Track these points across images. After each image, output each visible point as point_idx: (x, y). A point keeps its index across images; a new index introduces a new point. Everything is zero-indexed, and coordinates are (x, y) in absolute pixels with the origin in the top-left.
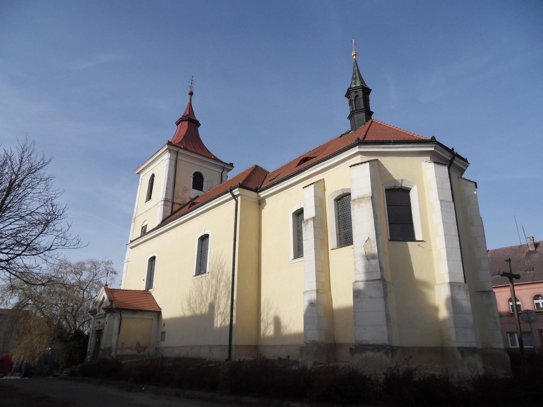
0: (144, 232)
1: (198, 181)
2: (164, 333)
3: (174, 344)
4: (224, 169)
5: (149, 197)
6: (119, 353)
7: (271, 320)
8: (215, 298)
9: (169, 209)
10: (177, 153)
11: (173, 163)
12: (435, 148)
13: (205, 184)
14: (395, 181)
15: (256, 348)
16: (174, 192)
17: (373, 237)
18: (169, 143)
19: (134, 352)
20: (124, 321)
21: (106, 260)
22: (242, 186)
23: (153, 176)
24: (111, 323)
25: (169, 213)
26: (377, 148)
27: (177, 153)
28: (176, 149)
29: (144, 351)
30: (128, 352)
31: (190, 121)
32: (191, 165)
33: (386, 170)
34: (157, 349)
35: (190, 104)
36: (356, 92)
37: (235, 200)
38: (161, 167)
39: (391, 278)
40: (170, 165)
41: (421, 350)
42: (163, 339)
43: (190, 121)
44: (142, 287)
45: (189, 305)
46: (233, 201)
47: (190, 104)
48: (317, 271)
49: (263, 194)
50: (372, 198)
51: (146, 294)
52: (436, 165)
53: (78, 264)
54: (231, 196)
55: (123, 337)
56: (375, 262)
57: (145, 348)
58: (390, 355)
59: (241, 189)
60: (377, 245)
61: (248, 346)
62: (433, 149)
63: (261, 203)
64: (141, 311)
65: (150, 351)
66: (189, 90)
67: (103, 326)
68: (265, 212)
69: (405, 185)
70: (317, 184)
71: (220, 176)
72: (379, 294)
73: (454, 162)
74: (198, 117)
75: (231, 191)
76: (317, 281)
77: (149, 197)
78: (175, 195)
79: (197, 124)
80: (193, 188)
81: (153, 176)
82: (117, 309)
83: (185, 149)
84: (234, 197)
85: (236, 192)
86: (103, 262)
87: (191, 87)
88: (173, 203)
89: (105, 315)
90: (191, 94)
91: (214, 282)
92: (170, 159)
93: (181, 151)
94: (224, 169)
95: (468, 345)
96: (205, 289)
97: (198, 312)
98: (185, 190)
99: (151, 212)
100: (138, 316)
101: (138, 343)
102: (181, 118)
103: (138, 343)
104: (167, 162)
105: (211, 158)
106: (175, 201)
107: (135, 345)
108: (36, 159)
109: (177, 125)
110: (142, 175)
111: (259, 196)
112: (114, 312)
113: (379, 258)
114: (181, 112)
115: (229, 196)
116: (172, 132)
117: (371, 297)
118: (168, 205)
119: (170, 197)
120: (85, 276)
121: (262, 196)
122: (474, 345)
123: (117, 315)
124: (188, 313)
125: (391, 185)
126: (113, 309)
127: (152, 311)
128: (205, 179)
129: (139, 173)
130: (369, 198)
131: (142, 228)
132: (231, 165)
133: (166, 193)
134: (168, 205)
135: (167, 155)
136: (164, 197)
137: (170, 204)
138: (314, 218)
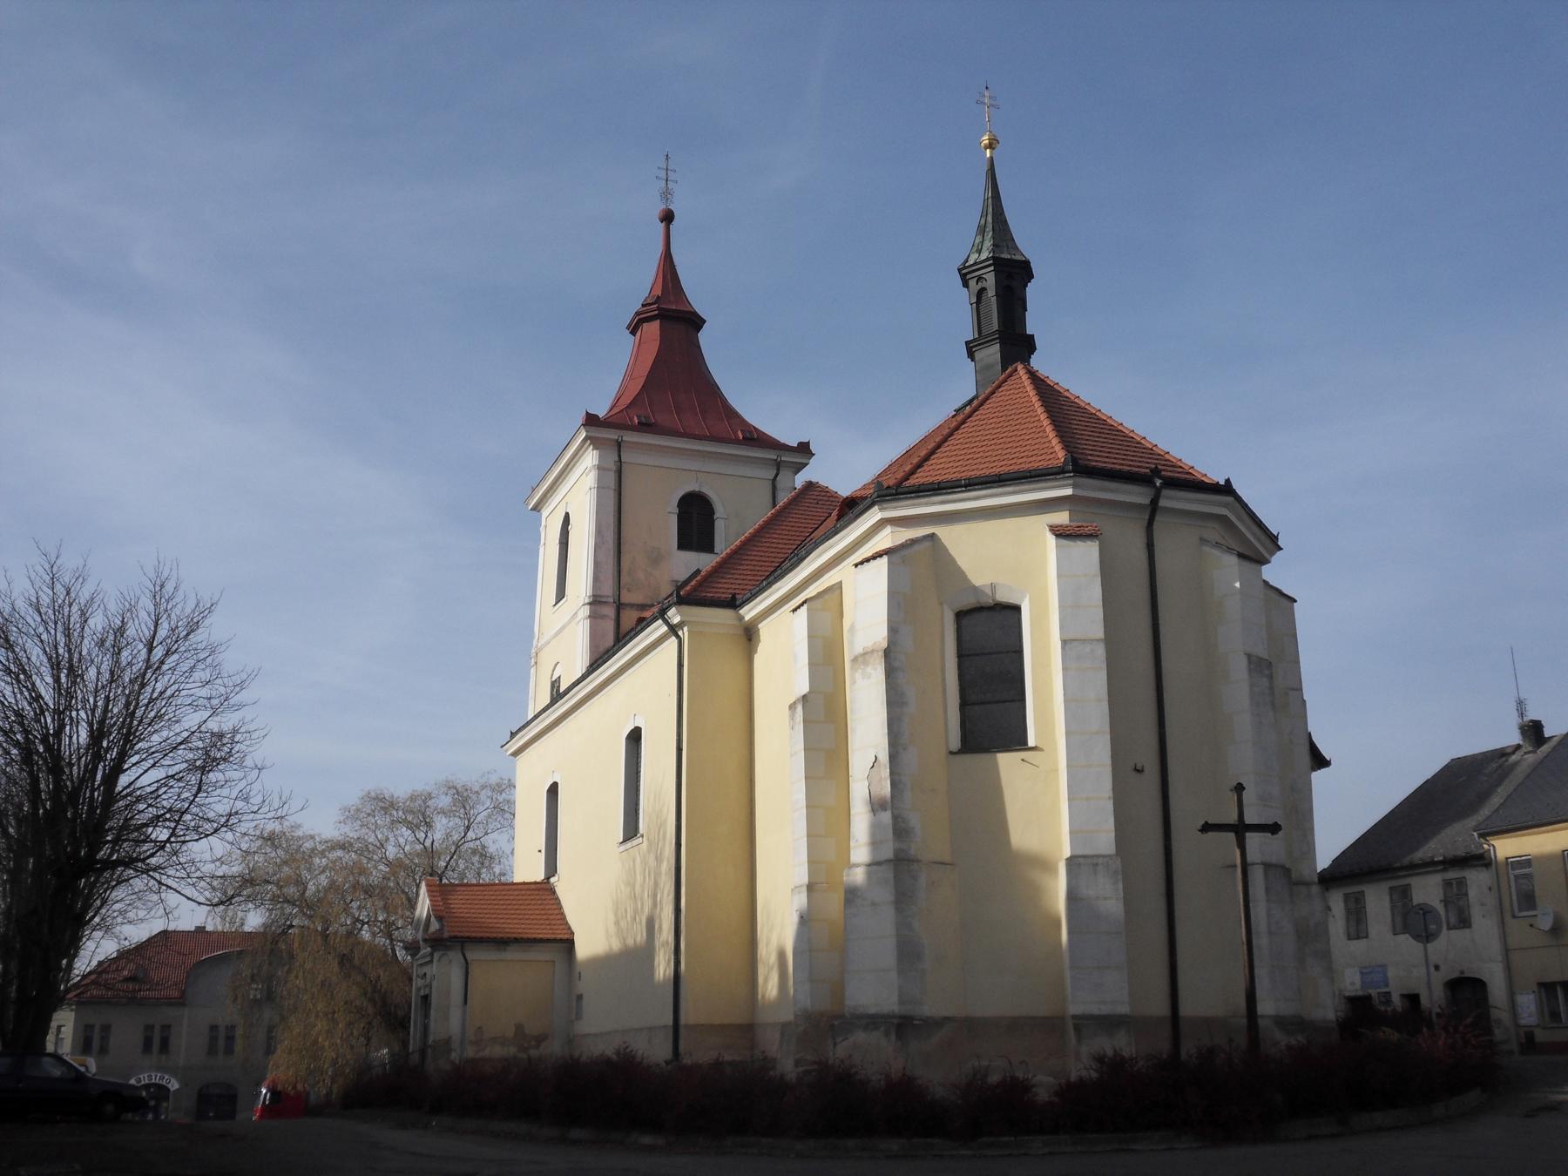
0: (557, 696)
1: (695, 522)
2: (580, 997)
3: (603, 1027)
4: (778, 465)
5: (561, 594)
6: (470, 1052)
7: (773, 958)
8: (655, 905)
9: (610, 626)
10: (619, 445)
11: (611, 479)
12: (1074, 486)
13: (720, 527)
14: (975, 589)
15: (748, 1030)
16: (619, 572)
17: (884, 757)
18: (591, 420)
19: (512, 1051)
20: (475, 971)
21: (494, 779)
22: (682, 601)
23: (567, 517)
24: (445, 974)
25: (610, 640)
26: (927, 504)
27: (619, 445)
28: (612, 435)
29: (537, 1047)
30: (497, 1051)
31: (671, 318)
32: (669, 472)
33: (952, 561)
34: (570, 1041)
35: (667, 258)
36: (980, 279)
37: (678, 636)
38: (579, 494)
39: (933, 852)
40: (600, 488)
41: (1015, 1025)
42: (579, 1016)
43: (671, 318)
44: (538, 875)
45: (617, 923)
46: (673, 641)
47: (667, 258)
48: (810, 836)
49: (749, 612)
50: (887, 653)
51: (544, 891)
52: (1064, 542)
53: (413, 798)
54: (665, 628)
55: (477, 1010)
56: (886, 817)
57: (540, 1039)
58: (893, 1037)
59: (685, 608)
60: (892, 773)
61: (722, 1027)
62: (1069, 491)
63: (749, 635)
64: (516, 940)
65: (554, 1049)
66: (659, 207)
67: (430, 986)
68: (759, 660)
69: (1003, 596)
70: (817, 604)
71: (769, 487)
72: (885, 895)
73: (1163, 503)
74: (698, 297)
75: (662, 614)
76: (812, 862)
77: (561, 594)
78: (625, 579)
79: (696, 322)
80: (682, 545)
81: (567, 517)
82: (454, 939)
83: (646, 427)
84: (673, 630)
85: (674, 616)
86: (483, 787)
87: (666, 195)
88: (620, 606)
89: (432, 955)
90: (668, 217)
91: (652, 861)
92: (600, 468)
93: (629, 437)
94: (778, 465)
95: (1105, 1010)
96: (639, 878)
97: (630, 942)
98: (656, 559)
99: (563, 633)
100: (511, 954)
101: (519, 1027)
102: (637, 314)
103: (519, 1027)
104: (590, 480)
105: (736, 442)
106: (627, 598)
107: (510, 1033)
108: (183, 608)
109: (633, 332)
110: (545, 512)
111: (741, 618)
112: (448, 948)
113: (893, 808)
114: (641, 283)
115: (659, 629)
116: (609, 369)
117: (873, 904)
118: (603, 617)
119: (608, 590)
120: (442, 829)
121: (747, 618)
122: (1123, 1009)
123: (455, 956)
124: (616, 945)
125: (968, 601)
126: (442, 940)
127: (548, 941)
128: (720, 511)
129: (537, 508)
130: (881, 654)
131: (553, 684)
132: (804, 449)
133: (596, 579)
134: (603, 617)
135: (590, 458)
136: (590, 592)
137: (610, 611)
138: (804, 697)
